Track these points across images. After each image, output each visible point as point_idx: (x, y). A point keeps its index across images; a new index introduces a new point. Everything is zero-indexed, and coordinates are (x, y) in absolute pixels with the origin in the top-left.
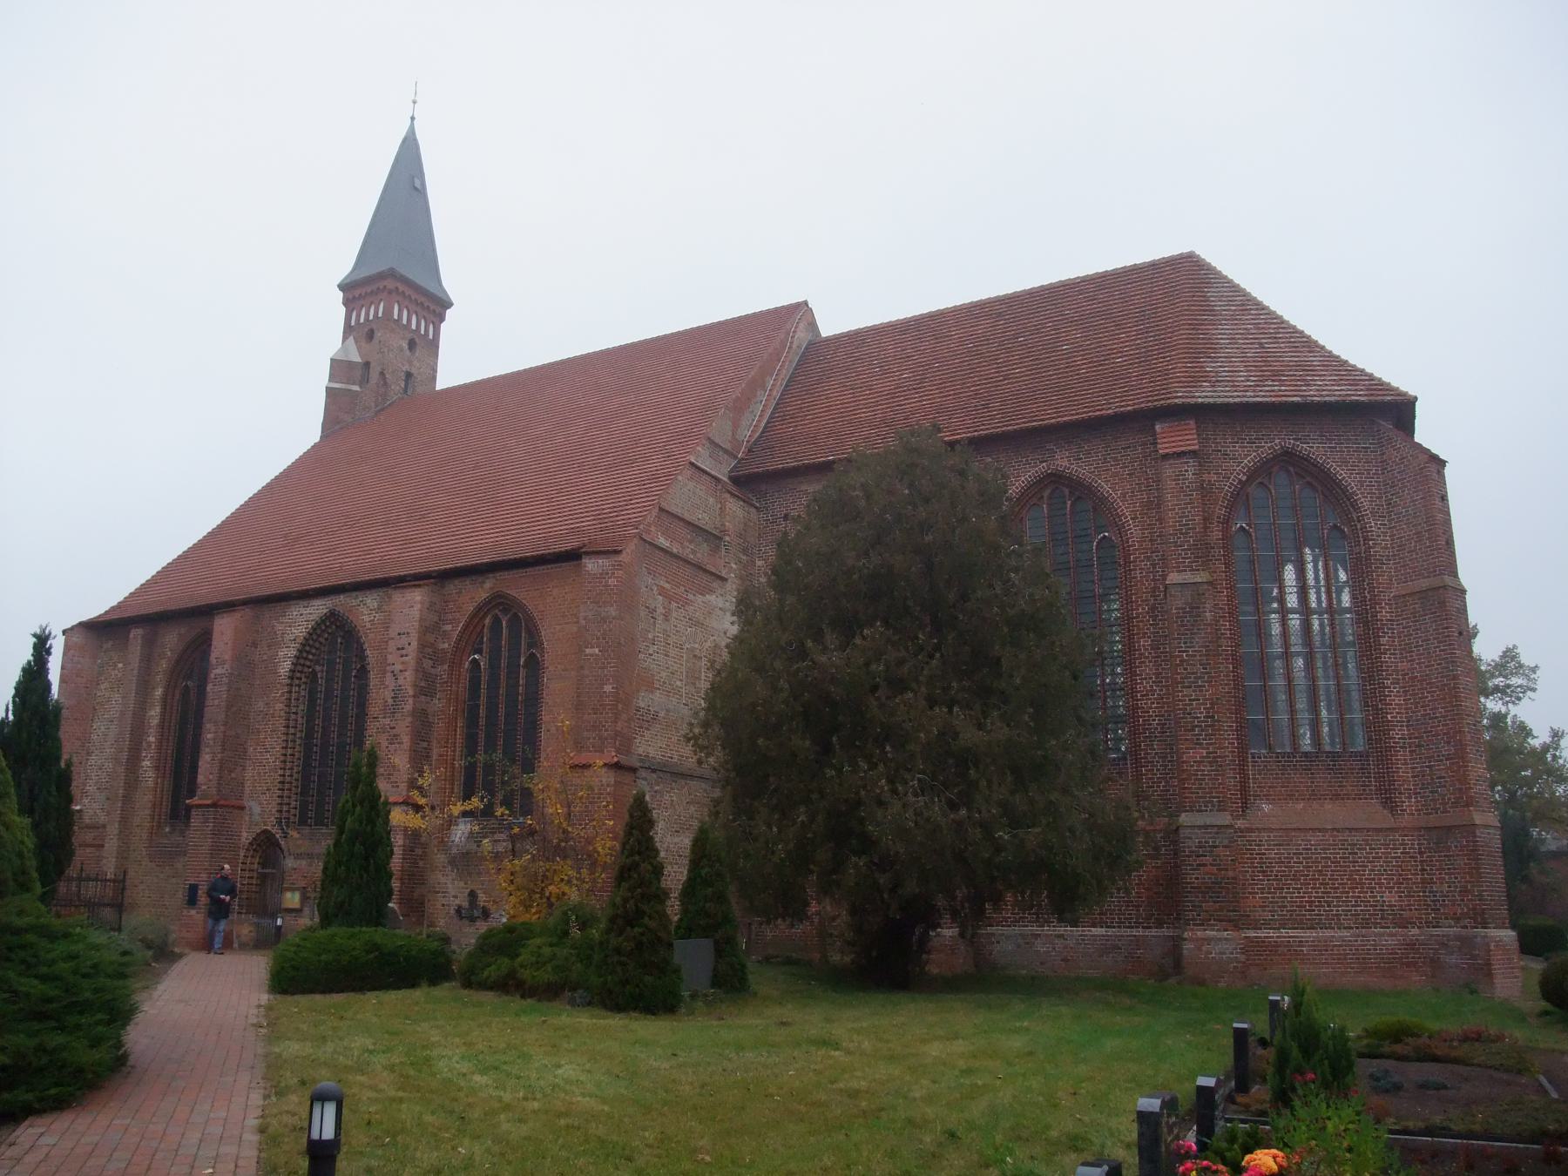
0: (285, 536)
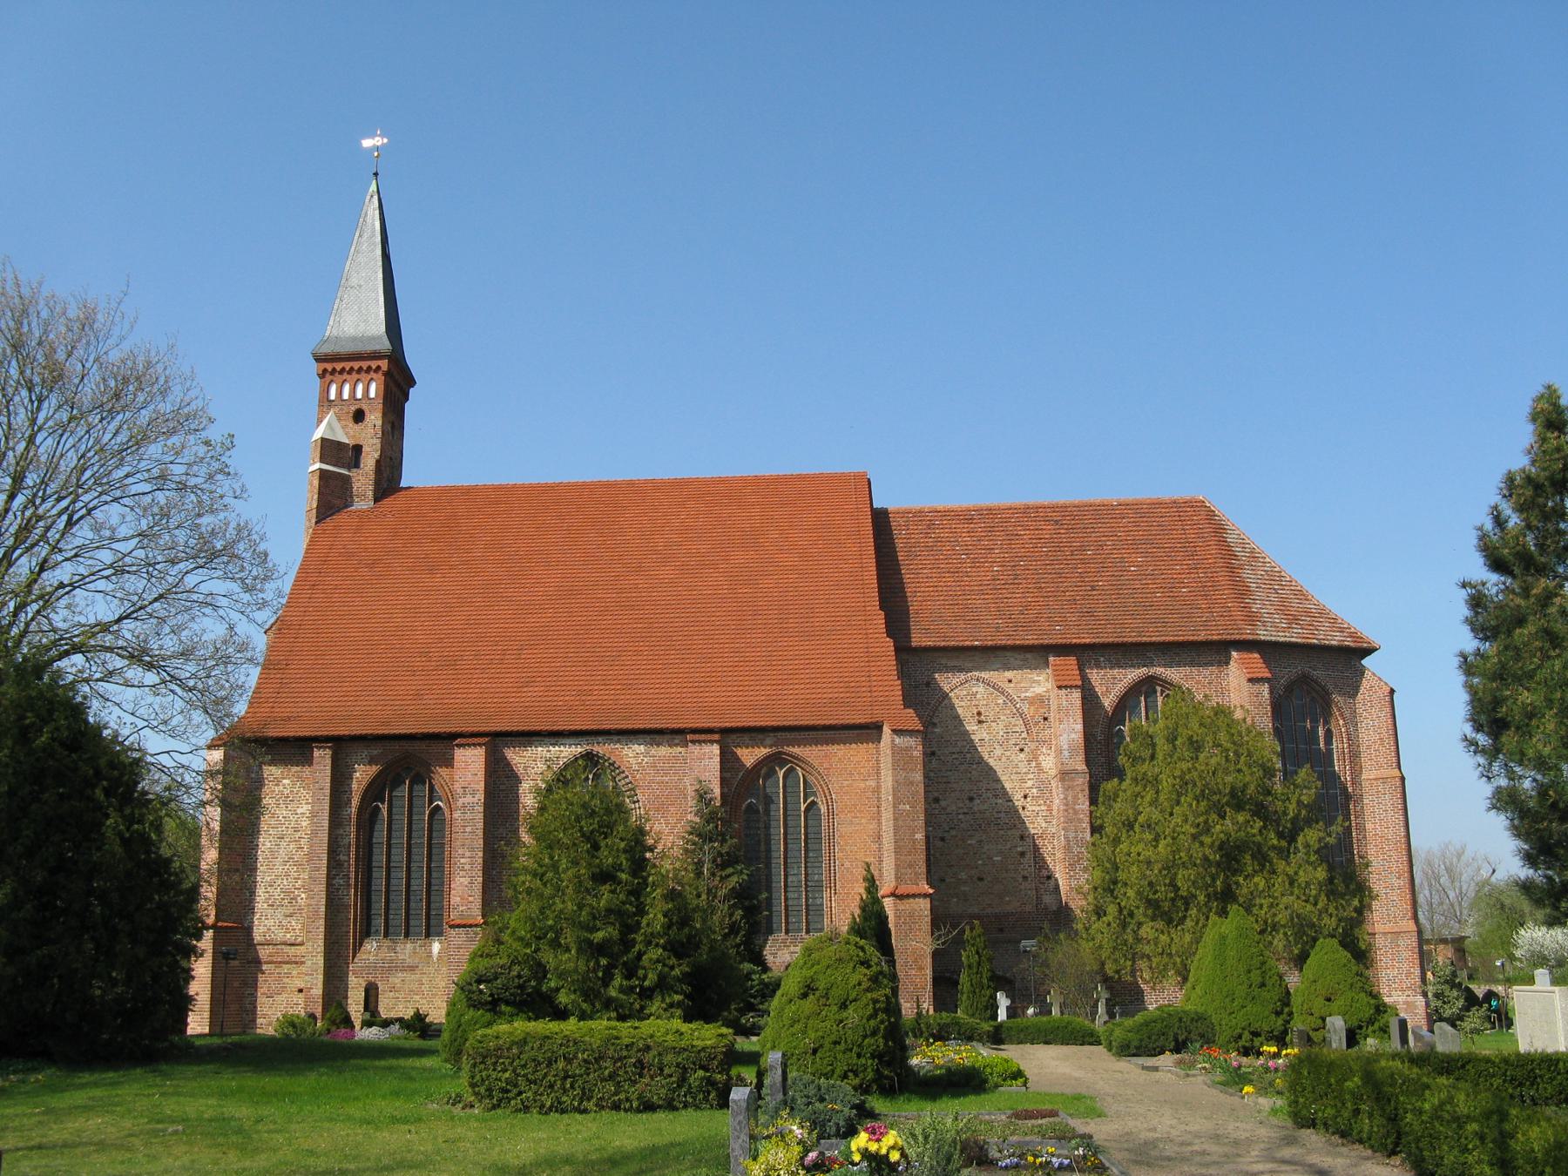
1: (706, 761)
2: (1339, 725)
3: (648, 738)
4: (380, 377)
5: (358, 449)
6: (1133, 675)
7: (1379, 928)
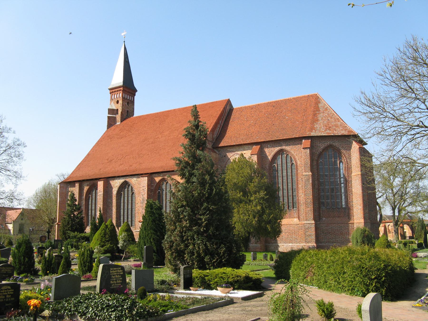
0: (108, 159)
1: (144, 181)
2: (344, 160)
3: (137, 176)
4: (121, 92)
5: (117, 110)
6: (277, 149)
7: (355, 221)
